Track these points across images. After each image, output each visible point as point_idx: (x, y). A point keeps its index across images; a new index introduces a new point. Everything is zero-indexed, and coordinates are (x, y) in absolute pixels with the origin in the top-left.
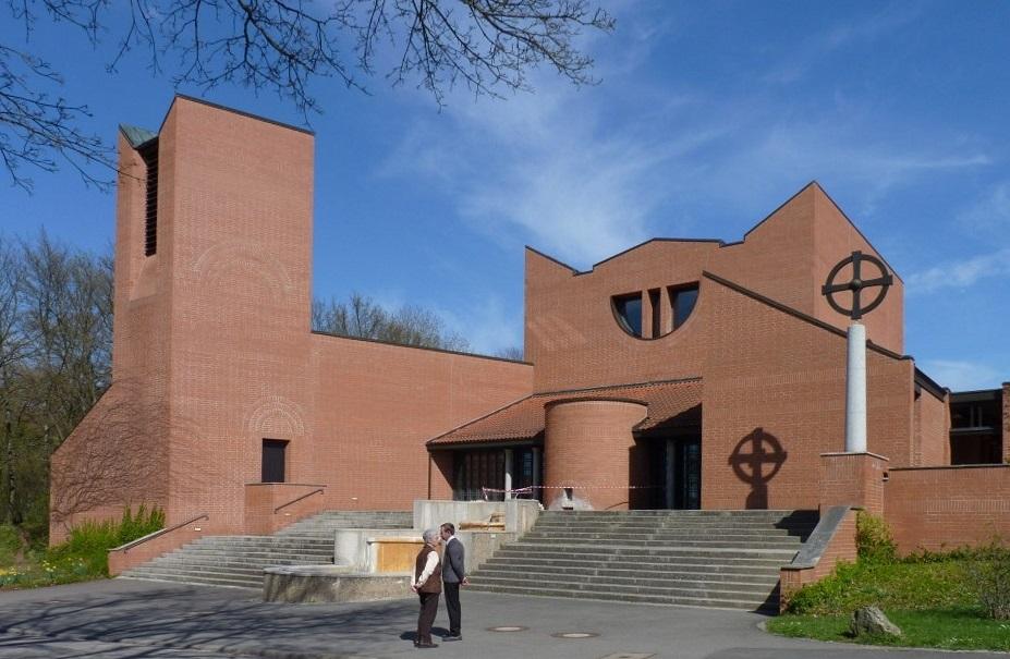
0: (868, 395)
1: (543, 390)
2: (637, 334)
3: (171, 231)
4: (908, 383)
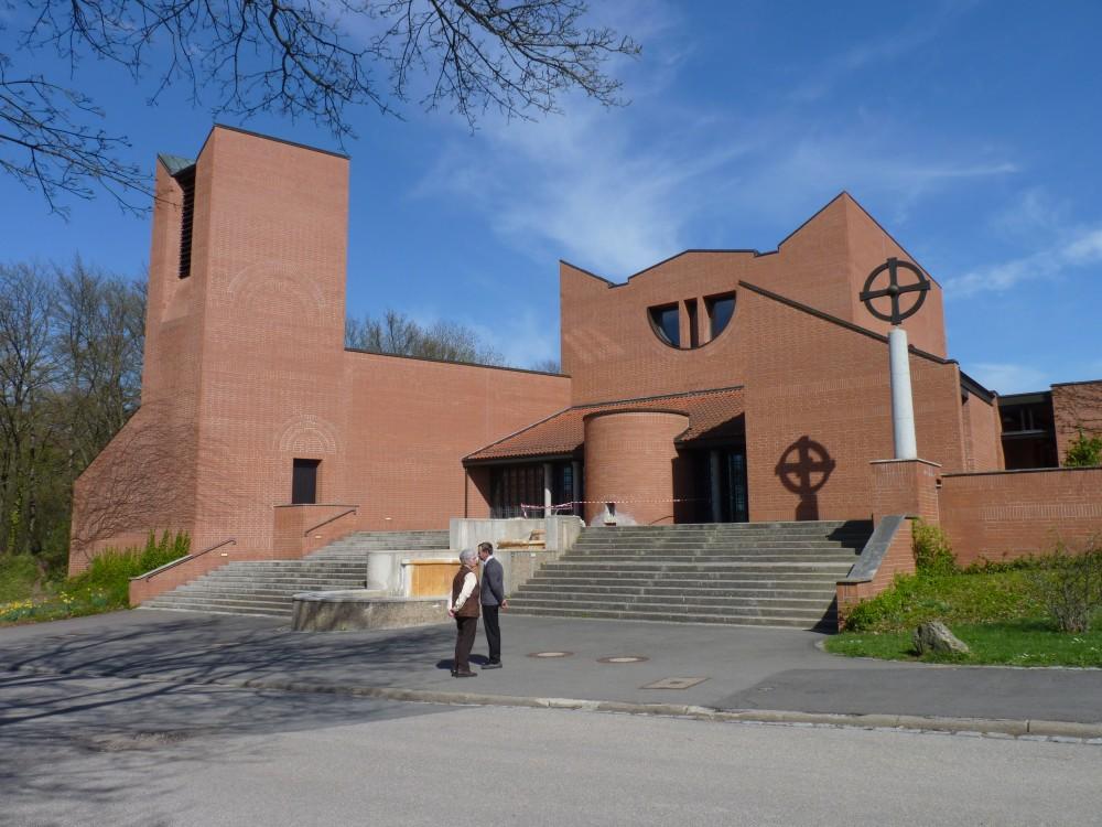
1: (582, 402)
2: (675, 344)
3: (205, 255)
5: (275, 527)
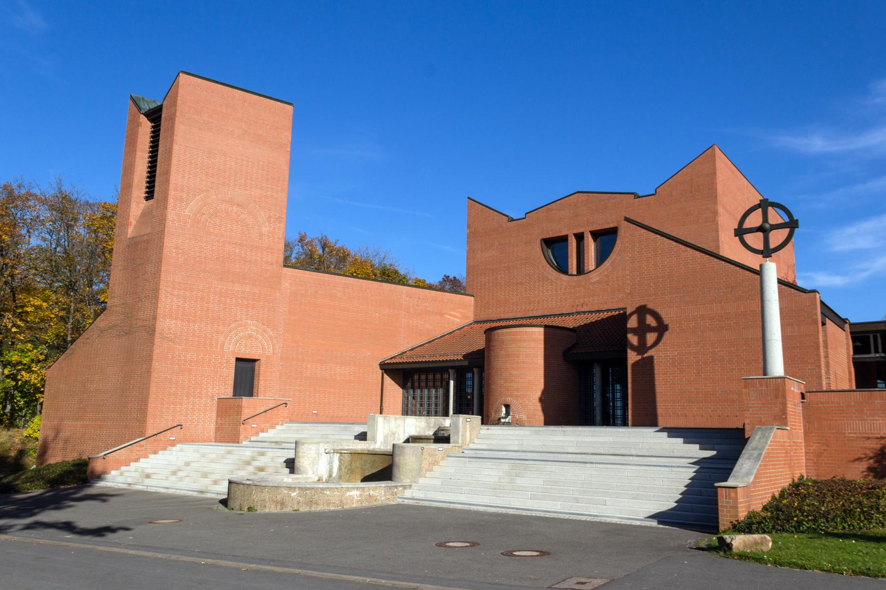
0: (782, 325)
1: (482, 318)
2: (563, 269)
3: (167, 181)
4: (816, 314)
5: (218, 416)
